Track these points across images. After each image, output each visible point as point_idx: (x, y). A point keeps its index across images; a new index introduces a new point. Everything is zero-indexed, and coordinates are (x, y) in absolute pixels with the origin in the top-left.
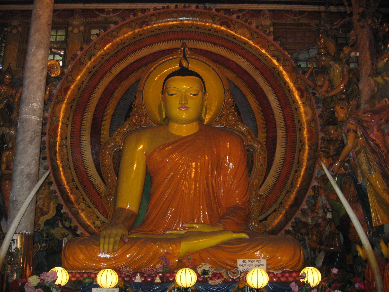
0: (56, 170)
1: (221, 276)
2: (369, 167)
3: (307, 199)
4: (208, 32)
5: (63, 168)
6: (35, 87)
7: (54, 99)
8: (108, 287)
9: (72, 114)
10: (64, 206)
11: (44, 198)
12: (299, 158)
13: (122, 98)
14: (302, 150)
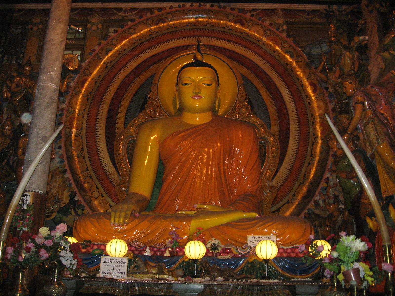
0: (70, 159)
1: (231, 252)
2: (376, 136)
3: (320, 191)
4: (222, 30)
5: (78, 157)
6: (54, 57)
7: (71, 91)
8: (117, 255)
9: (88, 106)
10: (78, 194)
11: (58, 187)
12: (312, 151)
13: (137, 92)
14: (314, 143)
